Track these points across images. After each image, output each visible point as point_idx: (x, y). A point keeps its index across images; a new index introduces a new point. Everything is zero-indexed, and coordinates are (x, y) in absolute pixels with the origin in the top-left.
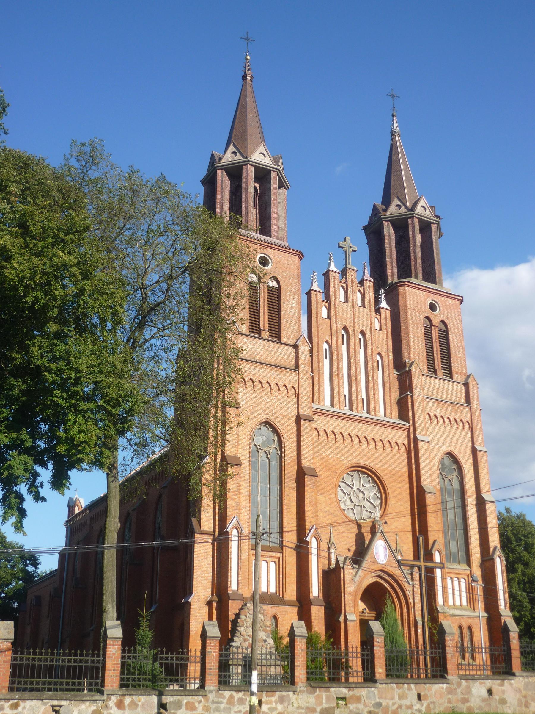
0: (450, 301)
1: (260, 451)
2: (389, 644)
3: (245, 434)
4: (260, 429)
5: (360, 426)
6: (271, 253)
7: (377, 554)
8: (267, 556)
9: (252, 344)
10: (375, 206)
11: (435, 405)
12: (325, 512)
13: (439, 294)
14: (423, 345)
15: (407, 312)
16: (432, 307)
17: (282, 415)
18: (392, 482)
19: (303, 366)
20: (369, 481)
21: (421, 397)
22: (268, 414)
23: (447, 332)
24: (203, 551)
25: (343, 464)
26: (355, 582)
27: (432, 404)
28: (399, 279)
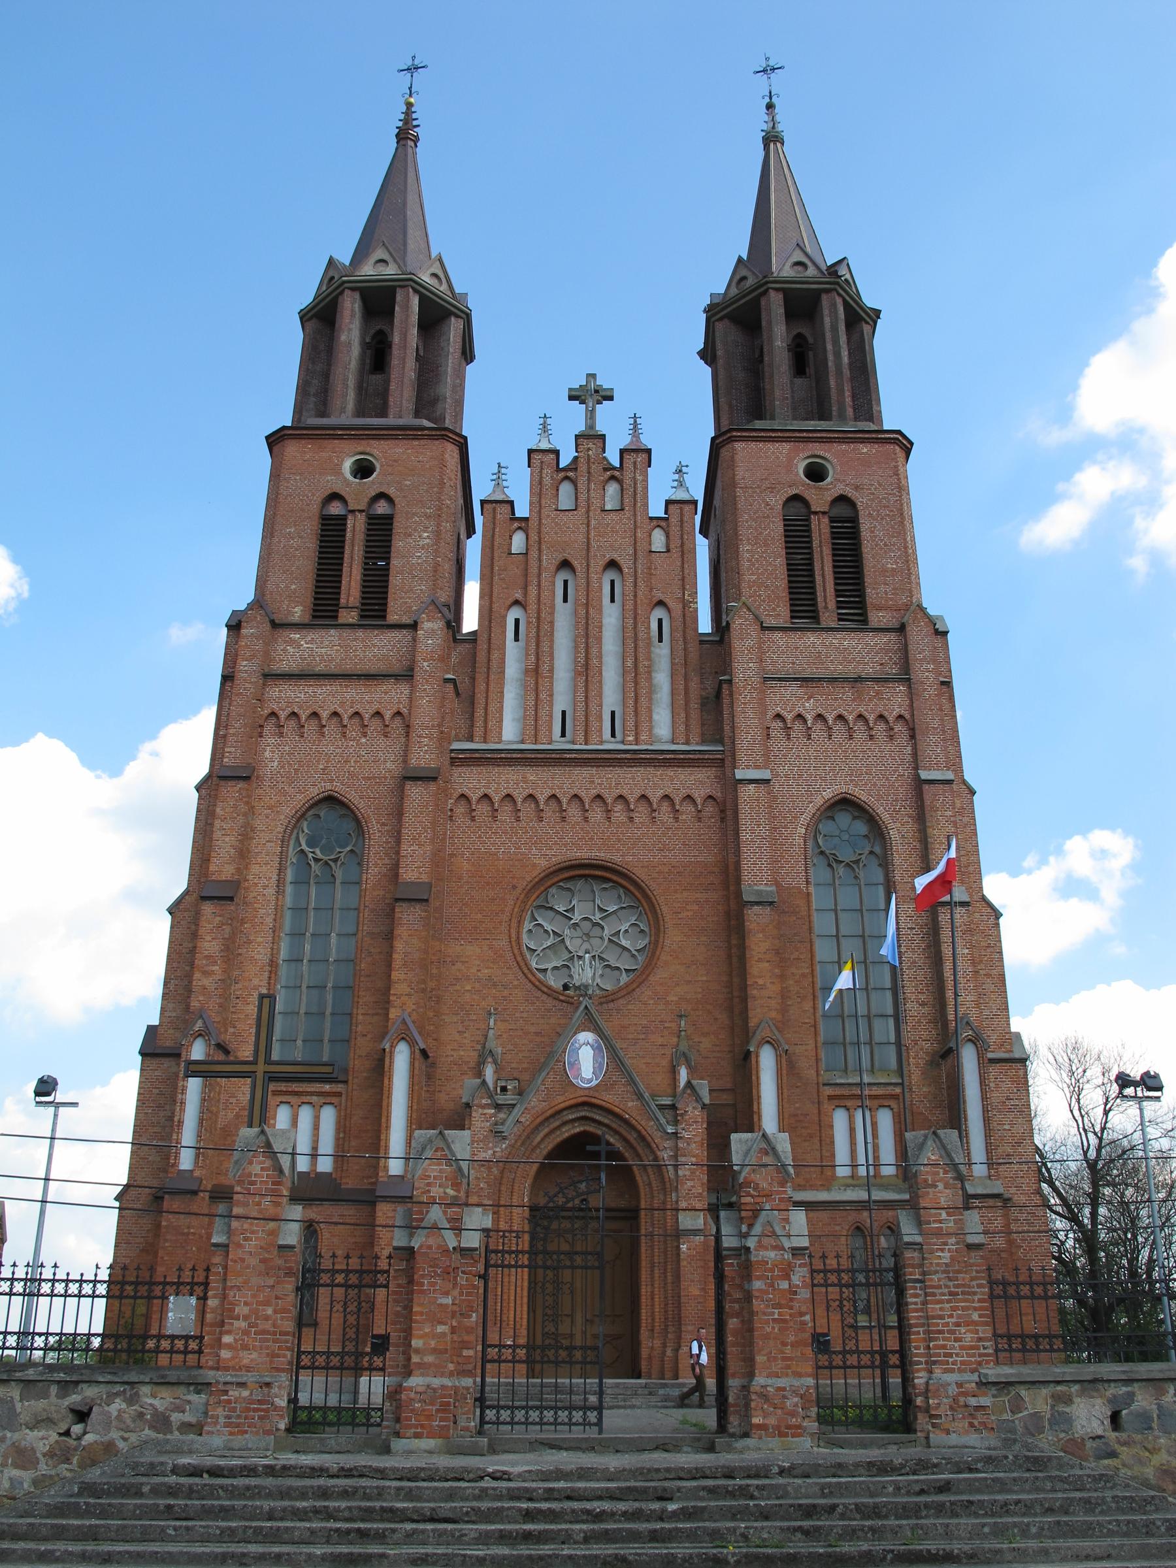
0: (864, 449)
1: (312, 863)
2: (118, 1271)
3: (272, 831)
4: (318, 816)
5: (639, 773)
6: (378, 451)
7: (572, 1065)
8: (312, 1094)
9: (312, 641)
10: (331, 262)
11: (800, 692)
12: (479, 980)
13: (830, 441)
14: (780, 562)
15: (735, 497)
16: (816, 473)
17: (369, 779)
18: (676, 891)
19: (425, 664)
20: (619, 897)
21: (756, 680)
22: (332, 781)
23: (854, 520)
24: (157, 1091)
25: (534, 865)
26: (505, 1138)
27: (792, 691)
28: (360, 412)
